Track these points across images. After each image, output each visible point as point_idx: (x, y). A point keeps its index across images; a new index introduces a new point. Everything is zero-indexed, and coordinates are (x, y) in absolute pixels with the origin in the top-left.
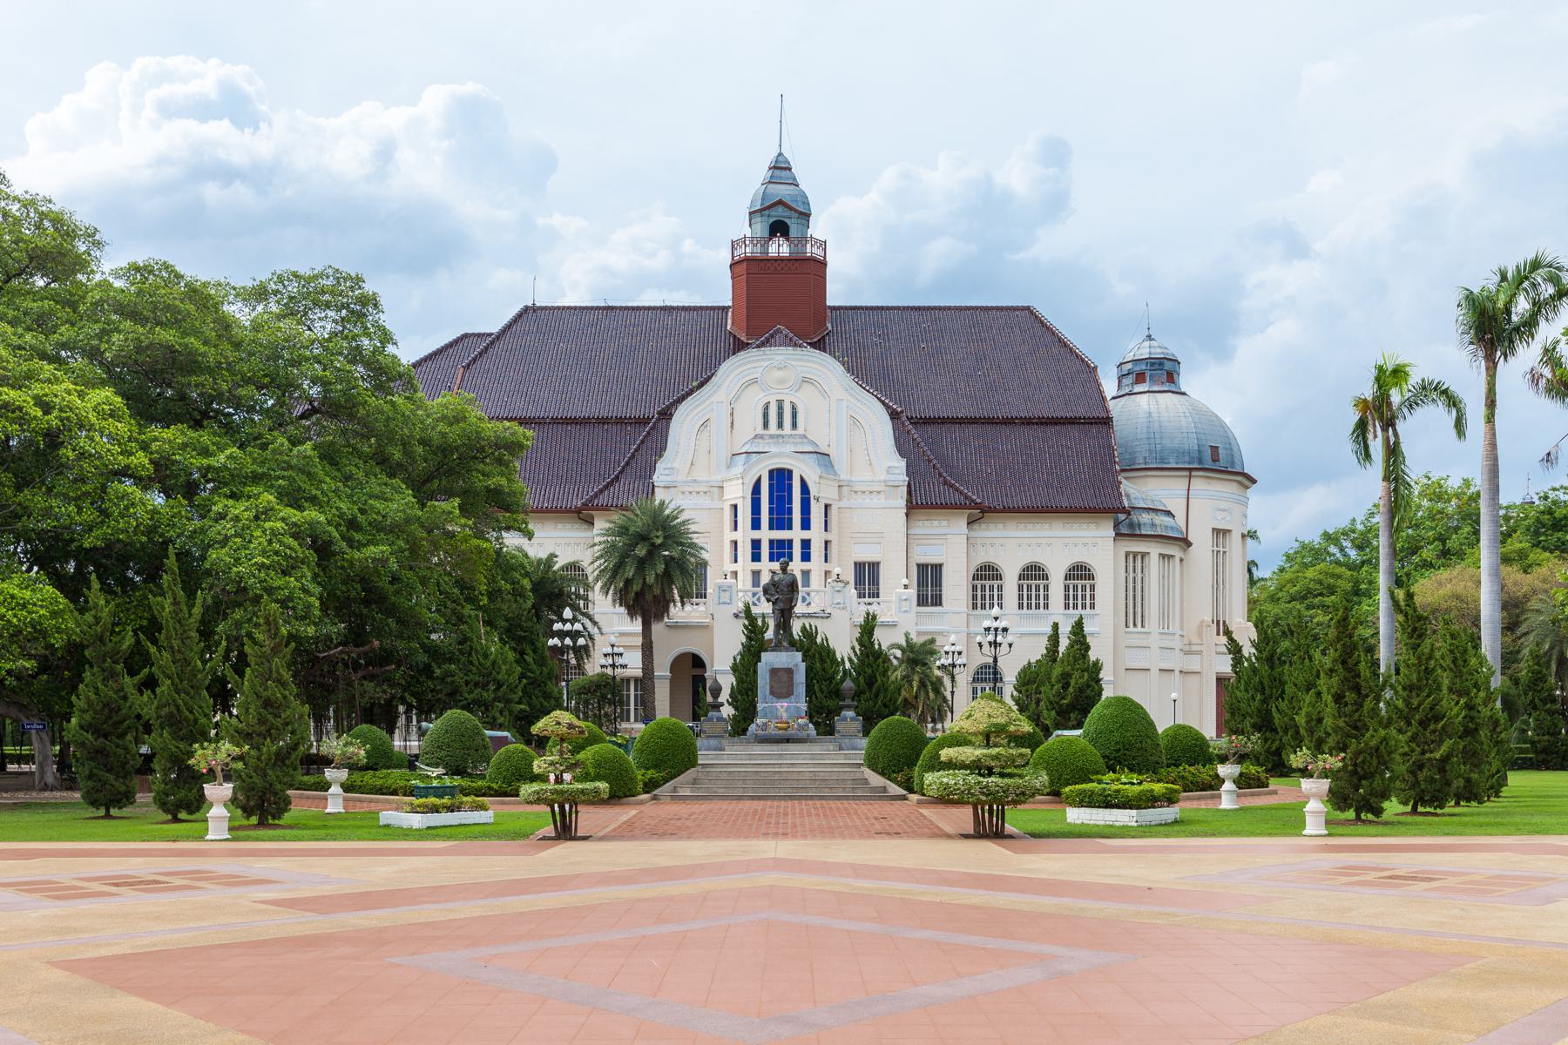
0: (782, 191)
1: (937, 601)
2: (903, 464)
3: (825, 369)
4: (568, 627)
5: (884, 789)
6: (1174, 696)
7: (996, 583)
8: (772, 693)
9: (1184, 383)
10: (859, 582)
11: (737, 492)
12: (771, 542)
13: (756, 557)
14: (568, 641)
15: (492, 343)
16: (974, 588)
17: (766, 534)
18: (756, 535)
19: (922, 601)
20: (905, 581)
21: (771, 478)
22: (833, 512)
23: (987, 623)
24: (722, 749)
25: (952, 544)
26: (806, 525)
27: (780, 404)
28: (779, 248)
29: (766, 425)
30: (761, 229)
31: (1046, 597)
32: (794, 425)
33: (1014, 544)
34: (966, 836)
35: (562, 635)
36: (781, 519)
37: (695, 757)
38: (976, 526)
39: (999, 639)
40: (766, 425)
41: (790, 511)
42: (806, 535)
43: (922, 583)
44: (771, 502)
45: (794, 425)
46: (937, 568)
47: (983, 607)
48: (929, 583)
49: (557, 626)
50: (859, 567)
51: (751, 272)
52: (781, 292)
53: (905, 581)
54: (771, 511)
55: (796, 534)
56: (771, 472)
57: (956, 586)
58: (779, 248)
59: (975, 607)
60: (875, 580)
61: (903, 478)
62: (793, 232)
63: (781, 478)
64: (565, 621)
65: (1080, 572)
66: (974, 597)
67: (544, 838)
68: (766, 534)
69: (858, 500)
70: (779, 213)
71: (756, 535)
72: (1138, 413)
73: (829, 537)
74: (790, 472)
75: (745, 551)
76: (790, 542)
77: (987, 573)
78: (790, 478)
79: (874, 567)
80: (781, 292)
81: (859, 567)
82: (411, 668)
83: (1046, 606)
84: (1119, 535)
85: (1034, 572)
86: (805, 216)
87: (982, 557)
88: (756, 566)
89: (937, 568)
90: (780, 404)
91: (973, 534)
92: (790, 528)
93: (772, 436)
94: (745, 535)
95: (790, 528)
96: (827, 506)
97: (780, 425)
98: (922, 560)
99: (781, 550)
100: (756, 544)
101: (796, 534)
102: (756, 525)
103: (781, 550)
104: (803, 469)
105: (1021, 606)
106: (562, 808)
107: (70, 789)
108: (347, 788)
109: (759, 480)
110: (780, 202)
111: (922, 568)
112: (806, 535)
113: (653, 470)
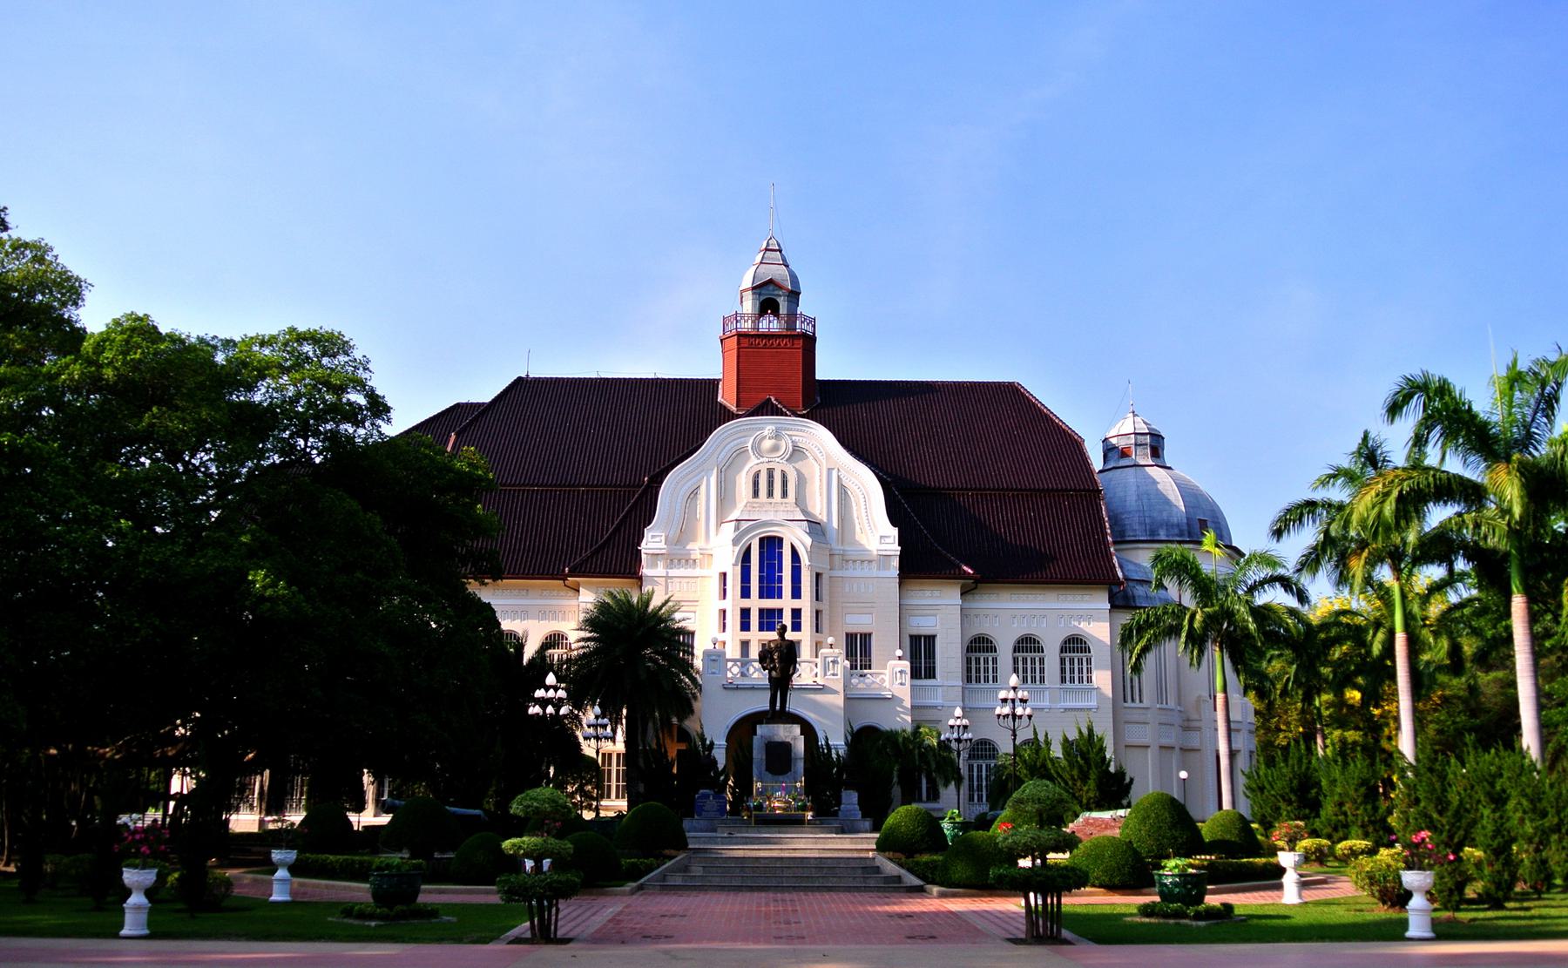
0: (778, 273)
1: (931, 674)
2: (895, 532)
3: (819, 439)
4: (551, 693)
5: (899, 879)
6: (1183, 775)
7: (1037, 655)
8: (768, 769)
9: (1168, 455)
10: (850, 654)
11: (724, 557)
12: (761, 611)
13: (745, 626)
14: (550, 710)
15: (476, 419)
16: (969, 661)
17: (756, 603)
18: (746, 603)
19: (915, 674)
20: (899, 653)
21: (761, 546)
22: (825, 580)
23: (1002, 694)
24: (715, 831)
25: (942, 610)
26: (796, 594)
27: (770, 473)
28: (770, 324)
29: (756, 494)
30: (749, 306)
31: (995, 670)
32: (785, 494)
33: (1014, 613)
34: (1016, 941)
35: (544, 703)
36: (770, 588)
37: (685, 839)
38: (969, 597)
39: (1019, 711)
40: (756, 494)
41: (780, 580)
42: (796, 604)
43: (914, 658)
44: (761, 570)
45: (785, 494)
46: (931, 639)
47: (978, 680)
48: (921, 655)
49: (539, 693)
50: (851, 638)
51: (748, 348)
52: (777, 366)
53: (899, 653)
54: (761, 579)
55: (786, 603)
56: (761, 540)
57: (949, 656)
58: (770, 324)
59: (969, 680)
60: (866, 651)
61: (895, 549)
62: (783, 310)
63: (771, 545)
64: (547, 689)
65: (1075, 645)
66: (969, 670)
67: (518, 940)
68: (756, 603)
69: (858, 572)
70: (768, 293)
71: (746, 603)
72: (1120, 488)
73: (821, 606)
74: (781, 540)
75: (733, 620)
76: (780, 611)
77: (979, 646)
78: (781, 546)
79: (866, 637)
80: (777, 366)
81: (851, 638)
82: (1363, 545)
83: (1042, 680)
84: (1114, 606)
85: (1027, 645)
86: (794, 295)
87: (975, 631)
88: (745, 635)
89: (931, 639)
90: (770, 473)
91: (967, 605)
92: (780, 597)
93: (762, 505)
94: (733, 603)
95: (780, 597)
96: (818, 575)
97: (770, 494)
98: (915, 632)
99: (769, 619)
100: (745, 613)
101: (786, 603)
102: (745, 593)
103: (769, 619)
104: (796, 537)
105: (1063, 680)
106: (540, 903)
107: (769, 629)
108: (295, 869)
109: (749, 549)
110: (771, 282)
111: (915, 640)
112: (796, 604)
113: (641, 537)
